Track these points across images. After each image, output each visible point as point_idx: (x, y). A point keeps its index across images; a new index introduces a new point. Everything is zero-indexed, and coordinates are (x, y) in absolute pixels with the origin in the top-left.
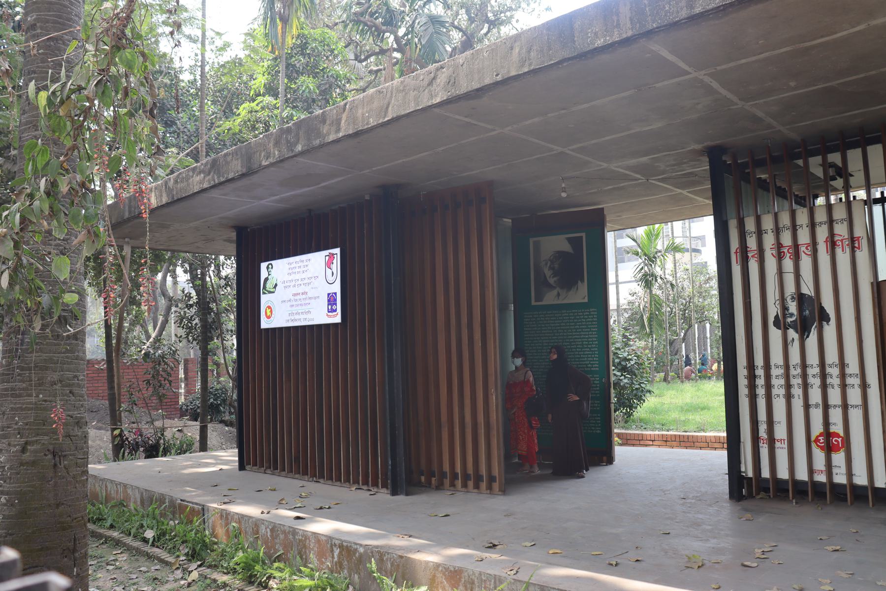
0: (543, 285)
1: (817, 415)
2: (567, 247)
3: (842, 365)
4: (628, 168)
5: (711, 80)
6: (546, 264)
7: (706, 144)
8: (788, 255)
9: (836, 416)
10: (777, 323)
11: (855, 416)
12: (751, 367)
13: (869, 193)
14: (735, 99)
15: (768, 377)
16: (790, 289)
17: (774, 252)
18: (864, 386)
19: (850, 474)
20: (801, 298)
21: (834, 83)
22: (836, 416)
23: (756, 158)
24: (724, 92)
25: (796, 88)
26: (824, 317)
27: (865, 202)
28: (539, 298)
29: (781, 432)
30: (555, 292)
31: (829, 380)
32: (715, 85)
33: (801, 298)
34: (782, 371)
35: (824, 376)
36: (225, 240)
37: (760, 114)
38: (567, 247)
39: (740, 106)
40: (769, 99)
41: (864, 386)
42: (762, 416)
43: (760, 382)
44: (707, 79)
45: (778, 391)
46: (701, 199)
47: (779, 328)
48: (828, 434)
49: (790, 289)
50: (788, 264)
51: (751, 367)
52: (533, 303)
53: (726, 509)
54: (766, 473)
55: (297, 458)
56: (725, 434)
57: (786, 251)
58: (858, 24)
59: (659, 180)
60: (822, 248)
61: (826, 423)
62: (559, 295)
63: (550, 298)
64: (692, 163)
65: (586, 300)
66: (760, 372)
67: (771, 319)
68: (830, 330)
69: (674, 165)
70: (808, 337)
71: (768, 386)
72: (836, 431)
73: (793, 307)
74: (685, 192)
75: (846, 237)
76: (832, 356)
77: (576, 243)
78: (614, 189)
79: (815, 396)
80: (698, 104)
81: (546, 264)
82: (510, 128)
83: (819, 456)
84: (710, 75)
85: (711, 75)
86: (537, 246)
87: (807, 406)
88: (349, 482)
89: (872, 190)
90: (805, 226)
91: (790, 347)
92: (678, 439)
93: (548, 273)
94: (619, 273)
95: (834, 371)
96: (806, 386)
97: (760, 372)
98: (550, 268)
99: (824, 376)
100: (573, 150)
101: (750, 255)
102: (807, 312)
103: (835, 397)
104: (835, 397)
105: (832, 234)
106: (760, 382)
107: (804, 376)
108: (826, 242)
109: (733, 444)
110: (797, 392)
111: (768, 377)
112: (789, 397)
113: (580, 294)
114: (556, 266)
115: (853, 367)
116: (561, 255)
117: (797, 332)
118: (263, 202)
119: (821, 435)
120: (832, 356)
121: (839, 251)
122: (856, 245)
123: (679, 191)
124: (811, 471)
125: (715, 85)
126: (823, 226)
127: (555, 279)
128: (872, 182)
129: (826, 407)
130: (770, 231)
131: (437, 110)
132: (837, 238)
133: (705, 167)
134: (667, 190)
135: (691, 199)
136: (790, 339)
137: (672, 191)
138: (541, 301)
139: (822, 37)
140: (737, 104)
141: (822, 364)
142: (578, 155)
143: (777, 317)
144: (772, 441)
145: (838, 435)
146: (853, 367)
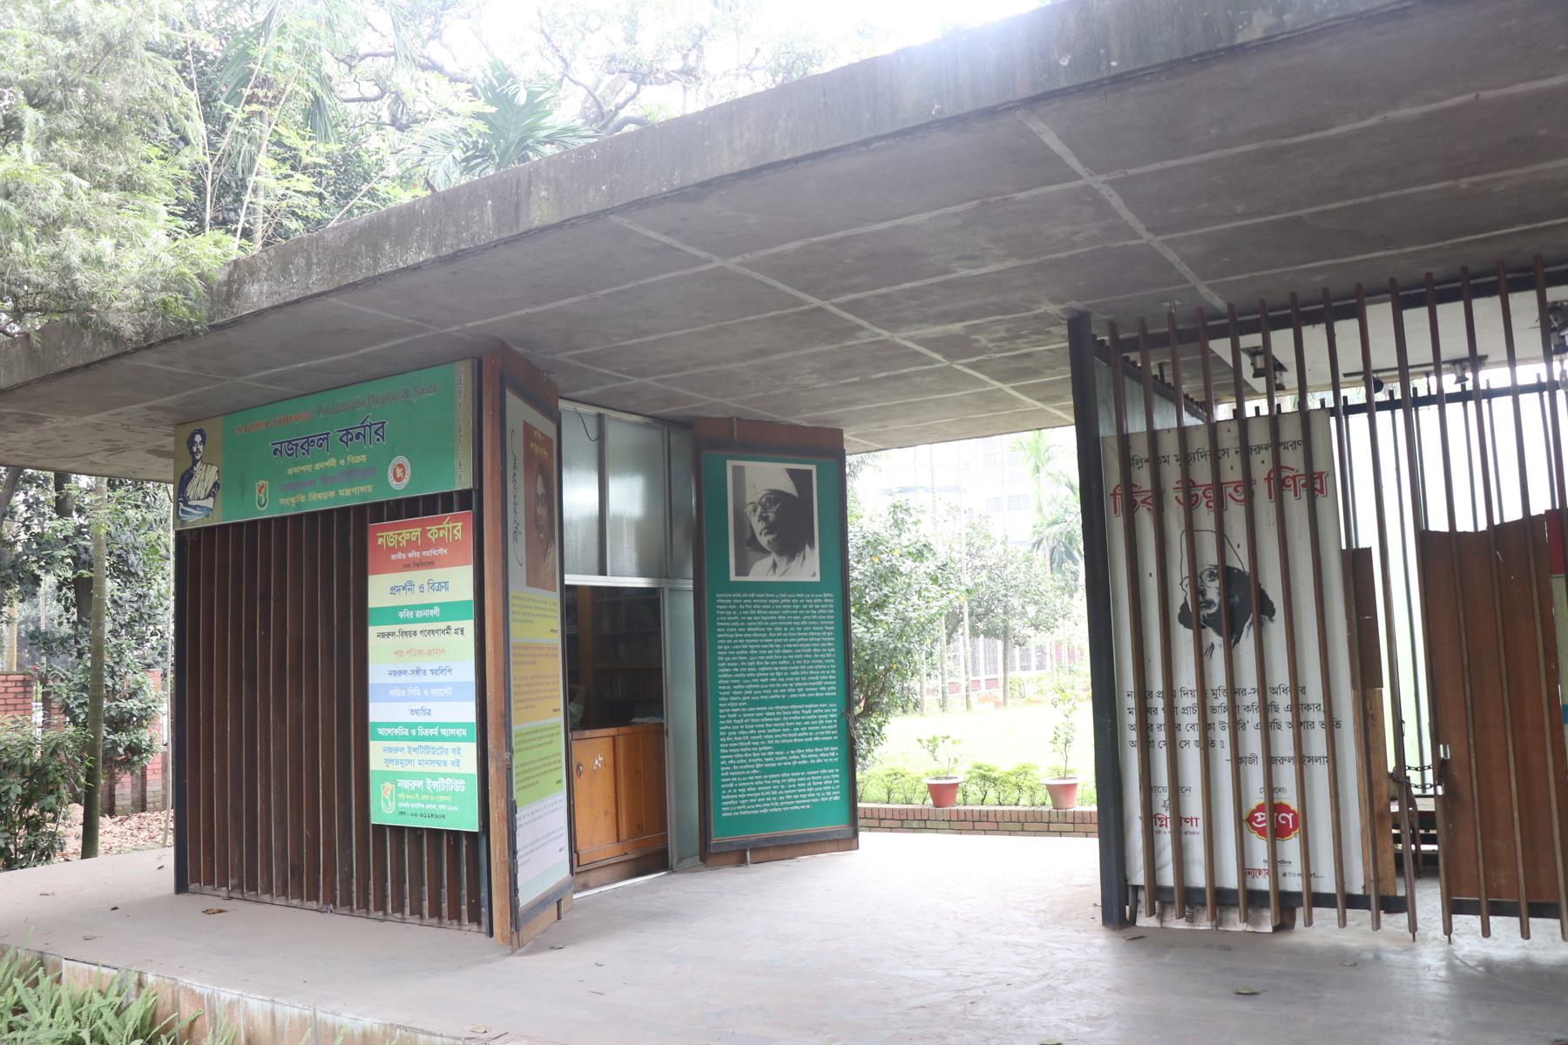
0: (748, 544)
1: (1255, 775)
2: (788, 486)
3: (1296, 689)
4: (924, 342)
5: (1112, 192)
6: (755, 510)
9: (1287, 775)
10: (1185, 619)
11: (1319, 774)
12: (1143, 693)
14: (1140, 227)
15: (1171, 710)
16: (1210, 557)
17: (1180, 496)
18: (1331, 725)
19: (1308, 875)
20: (1227, 575)
21: (1303, 212)
22: (1287, 775)
23: (1150, 332)
24: (1127, 215)
25: (1244, 216)
26: (1266, 608)
27: (1333, 412)
28: (743, 569)
29: (1194, 805)
30: (767, 562)
32: (1116, 201)
33: (1227, 575)
34: (1195, 700)
35: (1266, 708)
36: (149, 451)
37: (1172, 257)
38: (788, 486)
39: (1144, 241)
40: (1195, 232)
41: (1331, 725)
42: (1162, 777)
43: (1160, 718)
44: (1106, 191)
45: (1190, 735)
46: (1030, 401)
48: (1276, 808)
49: (1210, 557)
50: (1205, 518)
52: (733, 578)
53: (1094, 946)
54: (1168, 878)
55: (297, 870)
56: (1094, 808)
57: (1200, 493)
58: (1371, 114)
59: (972, 366)
61: (1270, 788)
62: (775, 566)
63: (761, 571)
64: (1034, 337)
65: (817, 579)
67: (1176, 610)
68: (1276, 630)
71: (1172, 727)
72: (1285, 802)
73: (1213, 591)
74: (1007, 388)
75: (1302, 471)
76: (1280, 674)
77: (800, 478)
79: (1253, 742)
80: (1077, 233)
81: (755, 510)
82: (738, 259)
83: (1259, 848)
84: (1112, 183)
86: (738, 471)
87: (1238, 761)
88: (440, 917)
89: (1309, 397)
90: (1232, 452)
91: (1206, 658)
92: (992, 818)
93: (758, 526)
95: (1283, 700)
96: (1236, 726)
97: (1159, 703)
98: (763, 518)
99: (1266, 708)
101: (1139, 499)
102: (1237, 599)
103: (1284, 742)
106: (1160, 718)
108: (1268, 479)
110: (1222, 736)
111: (1171, 710)
112: (1207, 744)
113: (808, 568)
114: (772, 516)
115: (1314, 694)
116: (776, 496)
118: (240, 380)
119: (1260, 808)
120: (1280, 674)
121: (1289, 495)
122: (1318, 486)
123: (998, 385)
124: (1245, 871)
125: (1116, 201)
127: (769, 537)
128: (1309, 383)
129: (1270, 761)
130: (1173, 460)
132: (1284, 474)
133: (1059, 343)
135: (1015, 400)
137: (985, 384)
138: (746, 574)
140: (1140, 238)
141: (1263, 688)
143: (1184, 606)
144: (1179, 821)
145: (1286, 809)
146: (1314, 694)
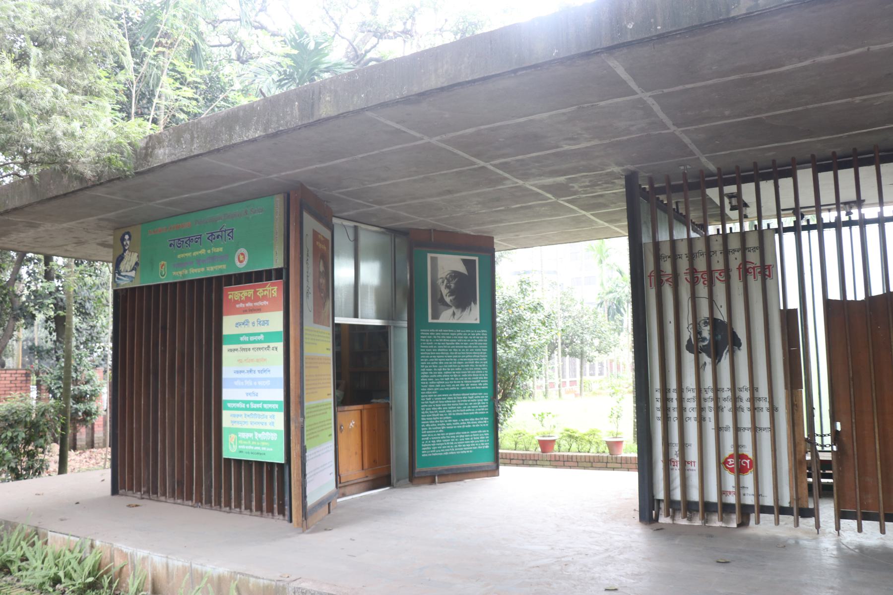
0: (440, 302)
2: (462, 269)
3: (753, 389)
4: (542, 187)
7: (625, 167)
8: (702, 280)
9: (746, 438)
10: (690, 348)
13: (779, 222)
14: (669, 123)
15: (681, 400)
16: (704, 313)
17: (688, 277)
18: (773, 410)
19: (758, 495)
20: (715, 323)
22: (746, 438)
23: (673, 183)
24: (662, 116)
25: (728, 117)
26: (736, 342)
28: (436, 316)
29: (693, 454)
30: (450, 312)
31: (739, 404)
32: (656, 108)
33: (715, 323)
34: (694, 394)
35: (735, 399)
38: (462, 269)
41: (773, 410)
43: (674, 404)
44: (651, 101)
46: (602, 222)
47: (691, 352)
48: (740, 457)
49: (704, 313)
51: (665, 390)
52: (430, 320)
56: (636, 455)
57: (699, 276)
58: (806, 59)
59: (568, 201)
60: (735, 275)
61: (737, 445)
62: (454, 314)
63: (446, 317)
64: (605, 186)
65: (478, 322)
66: (674, 395)
67: (684, 343)
68: (742, 355)
69: (588, 186)
70: (719, 361)
71: (681, 409)
72: (745, 453)
73: (706, 332)
74: (588, 214)
76: (744, 380)
77: (469, 264)
78: (521, 207)
79: (727, 419)
80: (633, 126)
82: (438, 138)
85: (654, 97)
86: (434, 260)
87: (719, 429)
93: (445, 291)
94: (306, 347)
95: (745, 395)
96: (718, 409)
97: (674, 395)
98: (447, 287)
99: (735, 399)
100: (494, 166)
101: (664, 279)
102: (720, 337)
104: (746, 419)
105: (745, 262)
106: (674, 404)
107: (717, 399)
108: (739, 268)
109: (645, 465)
110: (710, 415)
111: (681, 400)
112: (701, 420)
113: (473, 315)
114: (453, 286)
116: (455, 275)
117: (709, 356)
119: (731, 456)
120: (744, 380)
121: (751, 278)
122: (767, 273)
123: (584, 212)
124: (721, 492)
125: (656, 108)
126: (736, 253)
127: (451, 298)
128: (763, 214)
129: (737, 429)
130: (684, 257)
131: (369, 114)
132: (748, 266)
134: (572, 211)
135: (593, 221)
136: (701, 363)
139: (771, 68)
141: (734, 388)
142: (501, 172)
143: (689, 341)
144: (684, 463)
145: (746, 457)
146: (763, 392)
